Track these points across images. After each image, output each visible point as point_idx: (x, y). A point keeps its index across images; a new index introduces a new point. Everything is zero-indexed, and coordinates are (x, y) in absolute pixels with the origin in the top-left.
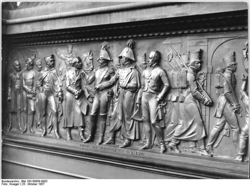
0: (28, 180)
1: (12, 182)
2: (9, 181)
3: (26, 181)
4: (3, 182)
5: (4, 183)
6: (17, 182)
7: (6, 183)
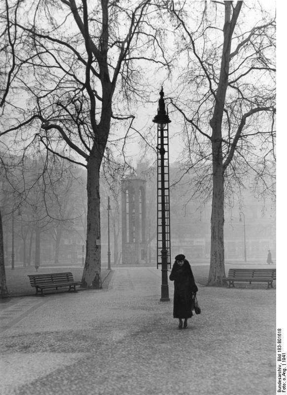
0: (277, 352)
2: (280, 381)
3: (280, 353)
4: (281, 390)
5: (282, 388)
7: (282, 385)
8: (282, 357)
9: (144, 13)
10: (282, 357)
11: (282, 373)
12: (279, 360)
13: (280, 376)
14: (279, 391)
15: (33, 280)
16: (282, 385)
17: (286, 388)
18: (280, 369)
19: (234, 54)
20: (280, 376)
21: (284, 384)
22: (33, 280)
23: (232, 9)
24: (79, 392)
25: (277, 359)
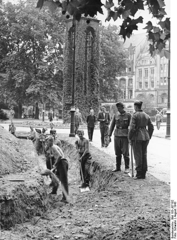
1: (173, 228)
2: (173, 232)
4: (174, 237)
5: (174, 236)
6: (173, 224)
7: (174, 234)
14: (172, 238)
16: (174, 234)
17: (176, 236)
21: (175, 234)
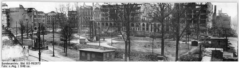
2: (8, 64)
4: (3, 65)
5: (4, 65)
7: (6, 65)
8: (23, 65)
9: (183, 53)
10: (23, 65)
11: (13, 65)
12: (21, 63)
13: (12, 64)
14: (2, 63)
15: (98, 20)
16: (6, 65)
18: (16, 64)
19: (93, 7)
20: (12, 64)
22: (98, 20)
23: (210, 36)
24: (51, 17)
25: (22, 62)
